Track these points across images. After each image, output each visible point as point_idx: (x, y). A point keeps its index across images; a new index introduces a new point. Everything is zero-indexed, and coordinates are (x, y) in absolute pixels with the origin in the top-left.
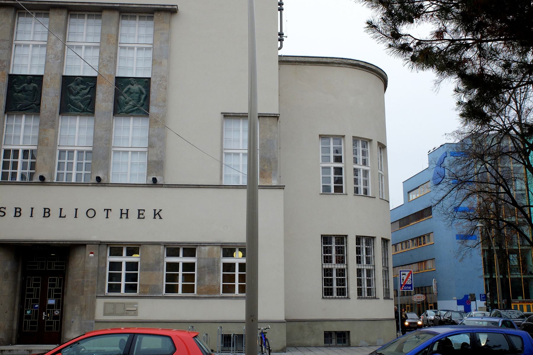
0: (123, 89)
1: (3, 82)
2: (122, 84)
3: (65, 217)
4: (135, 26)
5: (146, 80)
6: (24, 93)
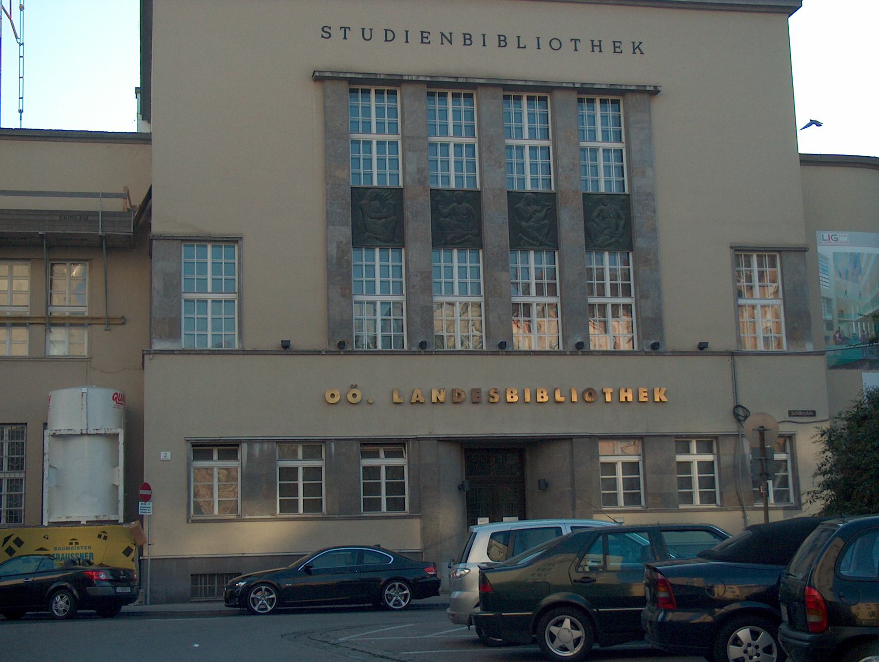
2: (590, 205)
3: (525, 47)
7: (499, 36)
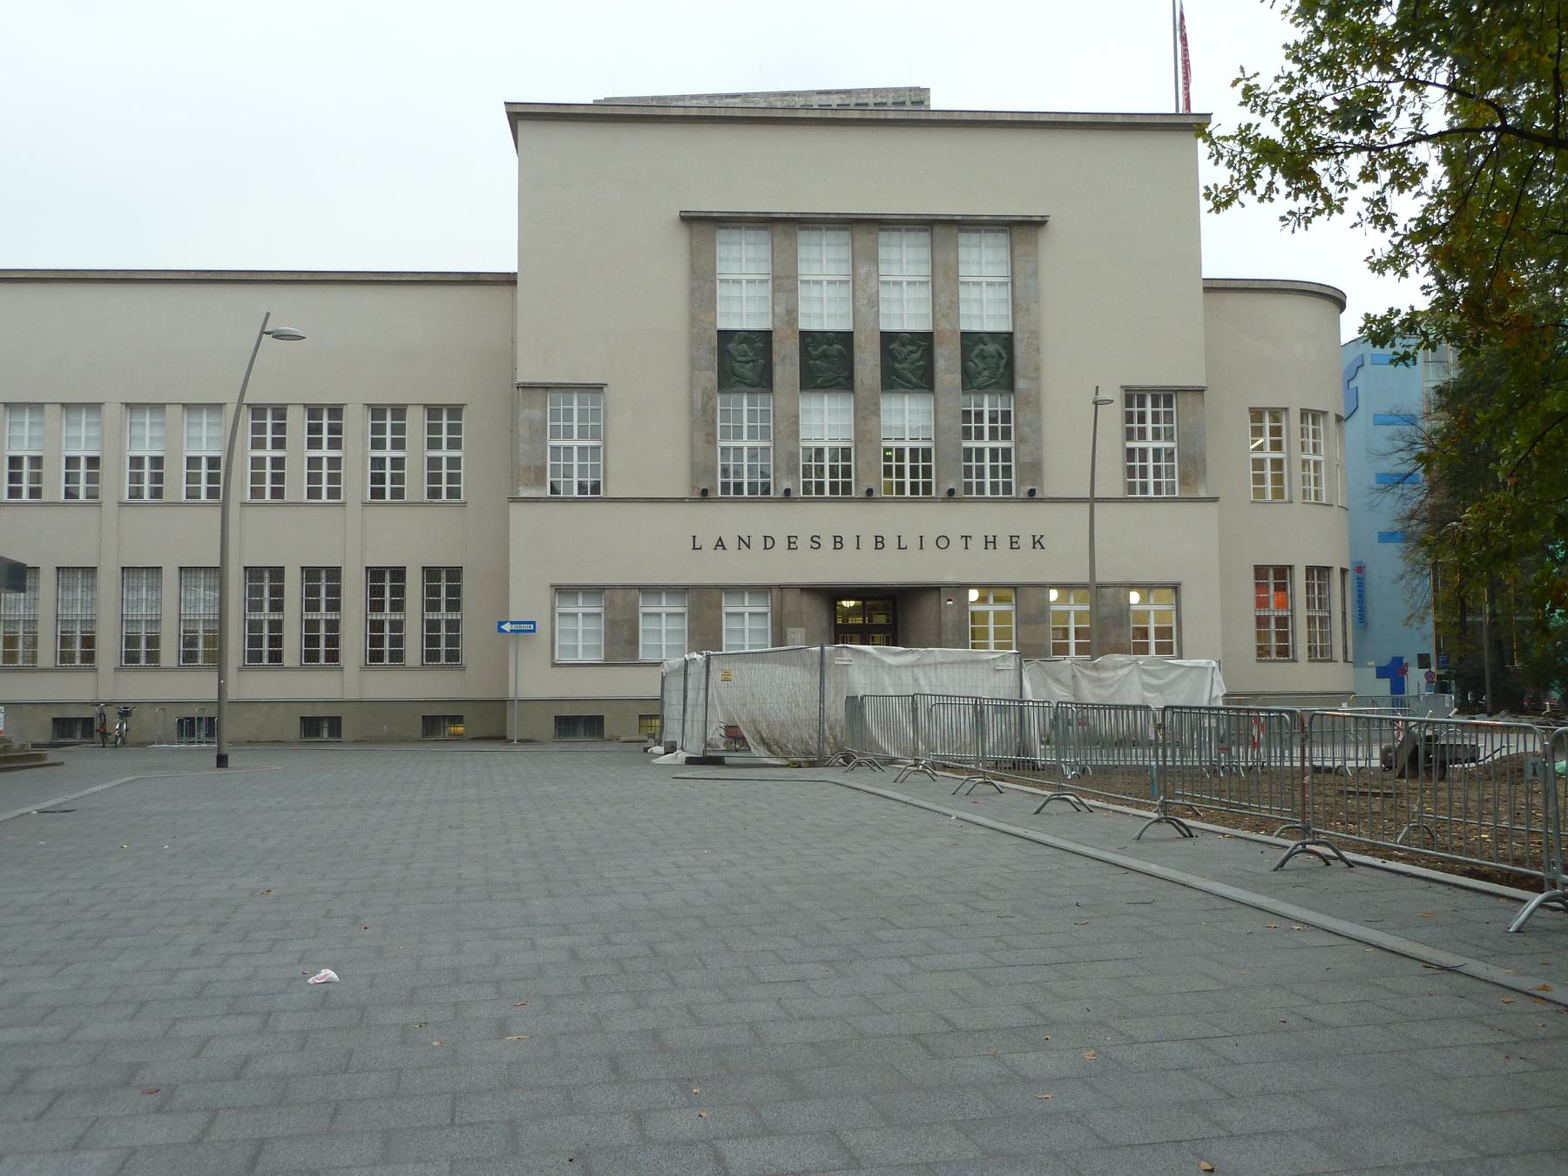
0: (972, 350)
1: (796, 344)
3: (906, 548)
4: (822, 245)
5: (1006, 335)
6: (824, 360)
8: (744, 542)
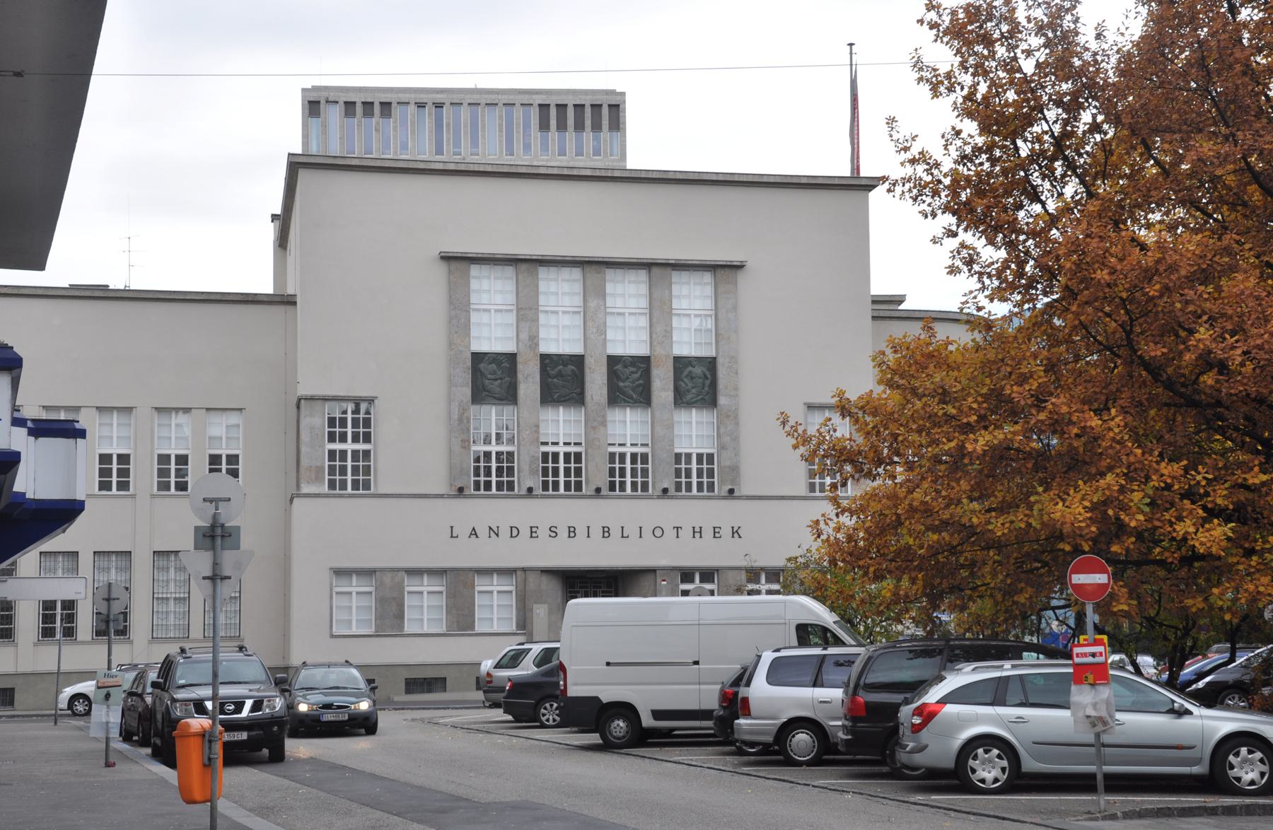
5: (710, 360)
7: (603, 528)
8: (494, 532)
